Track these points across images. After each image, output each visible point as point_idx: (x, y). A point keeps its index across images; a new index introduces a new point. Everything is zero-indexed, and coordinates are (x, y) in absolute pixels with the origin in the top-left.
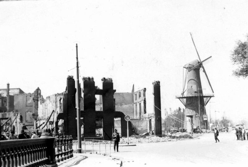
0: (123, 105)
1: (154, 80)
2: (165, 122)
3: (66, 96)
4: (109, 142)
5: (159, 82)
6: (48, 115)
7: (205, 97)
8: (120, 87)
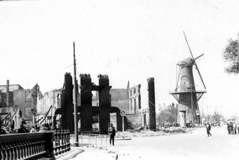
0: (118, 100)
1: (148, 77)
2: (159, 117)
3: (64, 92)
4: (105, 136)
5: (153, 79)
6: (46, 110)
7: (197, 93)
8: (115, 84)
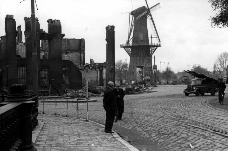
0: (68, 53)
5: (113, 27)
